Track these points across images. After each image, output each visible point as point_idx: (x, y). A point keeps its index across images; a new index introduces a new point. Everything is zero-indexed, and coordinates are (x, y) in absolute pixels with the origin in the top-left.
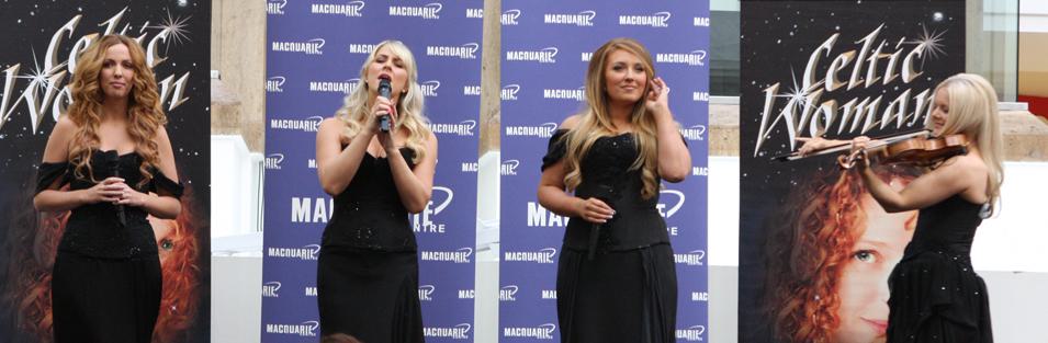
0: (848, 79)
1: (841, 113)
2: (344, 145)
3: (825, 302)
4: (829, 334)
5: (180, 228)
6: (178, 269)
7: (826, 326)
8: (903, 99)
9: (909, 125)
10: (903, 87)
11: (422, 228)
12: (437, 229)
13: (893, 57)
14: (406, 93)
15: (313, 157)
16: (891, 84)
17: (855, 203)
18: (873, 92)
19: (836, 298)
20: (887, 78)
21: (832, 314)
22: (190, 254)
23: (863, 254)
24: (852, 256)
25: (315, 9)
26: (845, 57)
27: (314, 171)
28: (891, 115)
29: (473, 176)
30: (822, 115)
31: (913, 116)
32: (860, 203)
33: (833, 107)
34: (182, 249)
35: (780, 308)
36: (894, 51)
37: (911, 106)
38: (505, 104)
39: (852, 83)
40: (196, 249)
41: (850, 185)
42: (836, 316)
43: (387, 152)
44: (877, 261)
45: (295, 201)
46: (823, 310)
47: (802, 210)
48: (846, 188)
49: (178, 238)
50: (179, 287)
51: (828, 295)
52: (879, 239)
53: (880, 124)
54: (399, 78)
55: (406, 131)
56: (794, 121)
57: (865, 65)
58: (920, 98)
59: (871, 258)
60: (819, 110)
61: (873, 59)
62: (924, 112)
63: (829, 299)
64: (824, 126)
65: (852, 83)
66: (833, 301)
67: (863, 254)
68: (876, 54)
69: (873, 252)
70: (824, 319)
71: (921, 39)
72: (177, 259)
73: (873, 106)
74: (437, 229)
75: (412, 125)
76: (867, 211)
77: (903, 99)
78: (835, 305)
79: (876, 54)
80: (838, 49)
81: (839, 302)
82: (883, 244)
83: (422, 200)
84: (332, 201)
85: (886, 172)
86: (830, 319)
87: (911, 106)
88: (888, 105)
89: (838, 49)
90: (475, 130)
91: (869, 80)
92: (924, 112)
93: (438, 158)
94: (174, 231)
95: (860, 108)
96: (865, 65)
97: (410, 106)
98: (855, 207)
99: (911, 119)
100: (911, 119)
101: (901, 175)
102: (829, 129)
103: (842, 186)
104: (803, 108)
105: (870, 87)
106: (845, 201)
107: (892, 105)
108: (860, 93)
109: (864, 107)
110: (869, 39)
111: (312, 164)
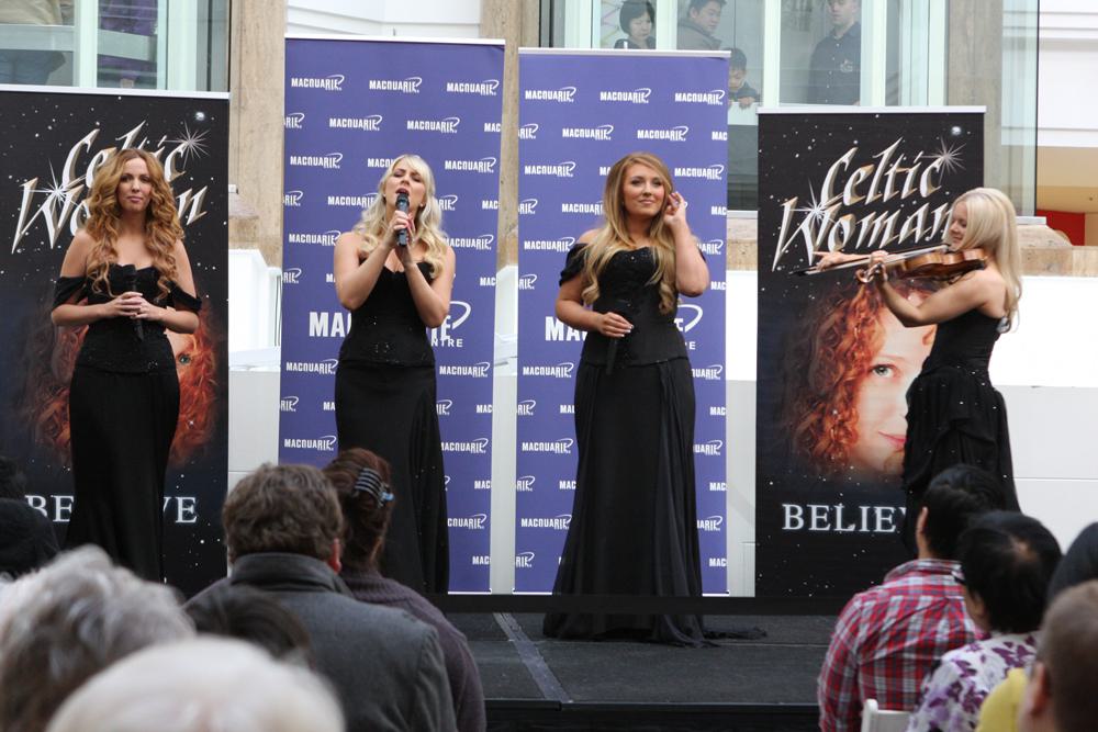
0: (866, 193)
1: (859, 227)
2: (362, 260)
3: (843, 416)
4: (847, 448)
5: (198, 343)
6: (196, 383)
7: (844, 441)
8: (921, 213)
9: (927, 239)
10: (922, 201)
11: (440, 342)
12: (455, 344)
13: (911, 172)
14: (424, 207)
15: (331, 272)
16: (909, 198)
17: (873, 318)
18: (891, 206)
19: (854, 412)
20: (906, 192)
21: (850, 429)
22: (208, 368)
23: (881, 369)
24: (870, 371)
25: (333, 123)
26: (863, 172)
27: (332, 285)
28: (909, 230)
29: (491, 290)
30: (840, 229)
31: (931, 230)
32: (878, 318)
33: (851, 222)
34: (200, 364)
35: (798, 422)
36: (912, 166)
37: (929, 220)
38: (494, 197)
39: (870, 197)
40: (213, 364)
41: (868, 299)
42: (854, 430)
43: (405, 267)
44: (895, 376)
45: (313, 316)
46: (841, 425)
47: (820, 325)
48: (864, 303)
49: (195, 353)
50: (197, 401)
51: (846, 409)
52: (897, 354)
53: (898, 238)
54: (417, 192)
55: (423, 245)
56: (812, 236)
57: (884, 179)
58: (938, 213)
59: (889, 373)
60: (837, 225)
61: (891, 173)
62: (942, 226)
63: (847, 414)
64: (842, 241)
65: (870, 197)
66: (851, 415)
67: (881, 369)
68: (894, 168)
69: (891, 366)
70: (842, 433)
71: (939, 154)
72: (195, 373)
73: (891, 221)
74: (455, 344)
75: (430, 239)
76: (885, 326)
77: (921, 213)
78: (853, 420)
79: (894, 168)
80: (856, 163)
81: (857, 417)
82: (901, 359)
83: (440, 314)
84: (349, 316)
85: (904, 286)
86: (848, 434)
87: (929, 220)
88: (906, 220)
89: (856, 163)
90: (493, 245)
91: (887, 195)
92: (942, 226)
93: (456, 272)
94: (192, 345)
95: (878, 222)
96: (884, 179)
97: (428, 220)
98: (873, 321)
99: (929, 234)
100: (929, 234)
101: (919, 289)
102: (847, 244)
103: (860, 300)
104: (821, 222)
105: (889, 201)
106: (863, 315)
107: (910, 219)
108: (879, 207)
109: (882, 222)
110: (887, 153)
111: (329, 278)
